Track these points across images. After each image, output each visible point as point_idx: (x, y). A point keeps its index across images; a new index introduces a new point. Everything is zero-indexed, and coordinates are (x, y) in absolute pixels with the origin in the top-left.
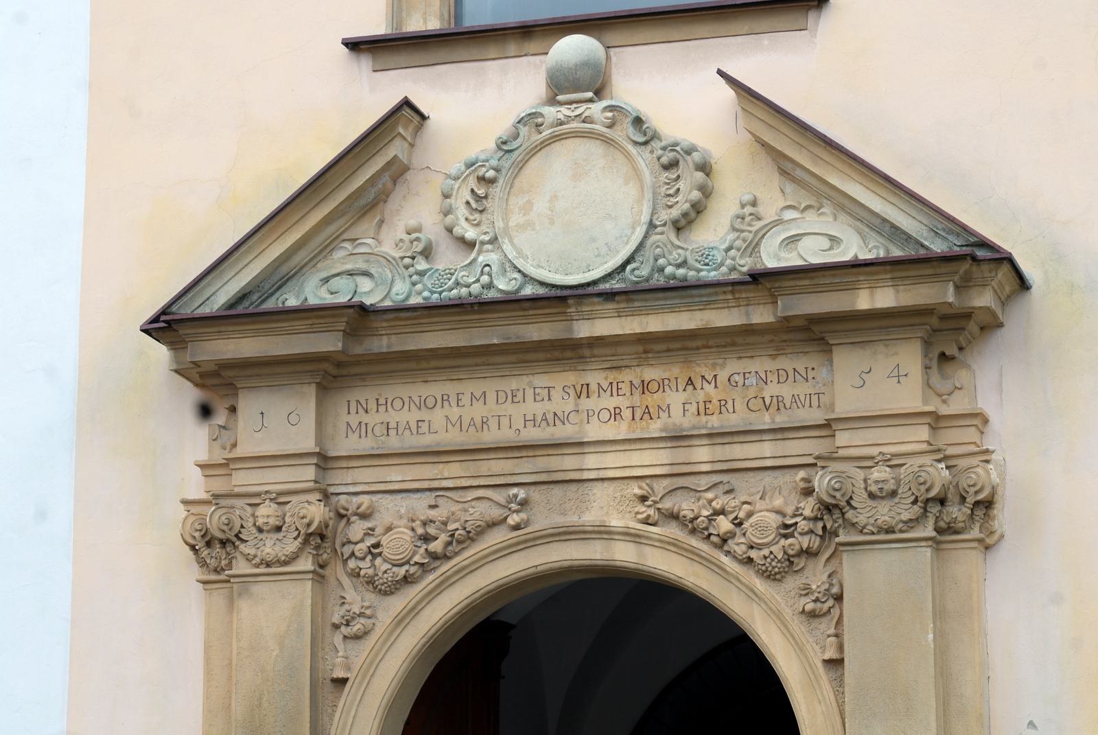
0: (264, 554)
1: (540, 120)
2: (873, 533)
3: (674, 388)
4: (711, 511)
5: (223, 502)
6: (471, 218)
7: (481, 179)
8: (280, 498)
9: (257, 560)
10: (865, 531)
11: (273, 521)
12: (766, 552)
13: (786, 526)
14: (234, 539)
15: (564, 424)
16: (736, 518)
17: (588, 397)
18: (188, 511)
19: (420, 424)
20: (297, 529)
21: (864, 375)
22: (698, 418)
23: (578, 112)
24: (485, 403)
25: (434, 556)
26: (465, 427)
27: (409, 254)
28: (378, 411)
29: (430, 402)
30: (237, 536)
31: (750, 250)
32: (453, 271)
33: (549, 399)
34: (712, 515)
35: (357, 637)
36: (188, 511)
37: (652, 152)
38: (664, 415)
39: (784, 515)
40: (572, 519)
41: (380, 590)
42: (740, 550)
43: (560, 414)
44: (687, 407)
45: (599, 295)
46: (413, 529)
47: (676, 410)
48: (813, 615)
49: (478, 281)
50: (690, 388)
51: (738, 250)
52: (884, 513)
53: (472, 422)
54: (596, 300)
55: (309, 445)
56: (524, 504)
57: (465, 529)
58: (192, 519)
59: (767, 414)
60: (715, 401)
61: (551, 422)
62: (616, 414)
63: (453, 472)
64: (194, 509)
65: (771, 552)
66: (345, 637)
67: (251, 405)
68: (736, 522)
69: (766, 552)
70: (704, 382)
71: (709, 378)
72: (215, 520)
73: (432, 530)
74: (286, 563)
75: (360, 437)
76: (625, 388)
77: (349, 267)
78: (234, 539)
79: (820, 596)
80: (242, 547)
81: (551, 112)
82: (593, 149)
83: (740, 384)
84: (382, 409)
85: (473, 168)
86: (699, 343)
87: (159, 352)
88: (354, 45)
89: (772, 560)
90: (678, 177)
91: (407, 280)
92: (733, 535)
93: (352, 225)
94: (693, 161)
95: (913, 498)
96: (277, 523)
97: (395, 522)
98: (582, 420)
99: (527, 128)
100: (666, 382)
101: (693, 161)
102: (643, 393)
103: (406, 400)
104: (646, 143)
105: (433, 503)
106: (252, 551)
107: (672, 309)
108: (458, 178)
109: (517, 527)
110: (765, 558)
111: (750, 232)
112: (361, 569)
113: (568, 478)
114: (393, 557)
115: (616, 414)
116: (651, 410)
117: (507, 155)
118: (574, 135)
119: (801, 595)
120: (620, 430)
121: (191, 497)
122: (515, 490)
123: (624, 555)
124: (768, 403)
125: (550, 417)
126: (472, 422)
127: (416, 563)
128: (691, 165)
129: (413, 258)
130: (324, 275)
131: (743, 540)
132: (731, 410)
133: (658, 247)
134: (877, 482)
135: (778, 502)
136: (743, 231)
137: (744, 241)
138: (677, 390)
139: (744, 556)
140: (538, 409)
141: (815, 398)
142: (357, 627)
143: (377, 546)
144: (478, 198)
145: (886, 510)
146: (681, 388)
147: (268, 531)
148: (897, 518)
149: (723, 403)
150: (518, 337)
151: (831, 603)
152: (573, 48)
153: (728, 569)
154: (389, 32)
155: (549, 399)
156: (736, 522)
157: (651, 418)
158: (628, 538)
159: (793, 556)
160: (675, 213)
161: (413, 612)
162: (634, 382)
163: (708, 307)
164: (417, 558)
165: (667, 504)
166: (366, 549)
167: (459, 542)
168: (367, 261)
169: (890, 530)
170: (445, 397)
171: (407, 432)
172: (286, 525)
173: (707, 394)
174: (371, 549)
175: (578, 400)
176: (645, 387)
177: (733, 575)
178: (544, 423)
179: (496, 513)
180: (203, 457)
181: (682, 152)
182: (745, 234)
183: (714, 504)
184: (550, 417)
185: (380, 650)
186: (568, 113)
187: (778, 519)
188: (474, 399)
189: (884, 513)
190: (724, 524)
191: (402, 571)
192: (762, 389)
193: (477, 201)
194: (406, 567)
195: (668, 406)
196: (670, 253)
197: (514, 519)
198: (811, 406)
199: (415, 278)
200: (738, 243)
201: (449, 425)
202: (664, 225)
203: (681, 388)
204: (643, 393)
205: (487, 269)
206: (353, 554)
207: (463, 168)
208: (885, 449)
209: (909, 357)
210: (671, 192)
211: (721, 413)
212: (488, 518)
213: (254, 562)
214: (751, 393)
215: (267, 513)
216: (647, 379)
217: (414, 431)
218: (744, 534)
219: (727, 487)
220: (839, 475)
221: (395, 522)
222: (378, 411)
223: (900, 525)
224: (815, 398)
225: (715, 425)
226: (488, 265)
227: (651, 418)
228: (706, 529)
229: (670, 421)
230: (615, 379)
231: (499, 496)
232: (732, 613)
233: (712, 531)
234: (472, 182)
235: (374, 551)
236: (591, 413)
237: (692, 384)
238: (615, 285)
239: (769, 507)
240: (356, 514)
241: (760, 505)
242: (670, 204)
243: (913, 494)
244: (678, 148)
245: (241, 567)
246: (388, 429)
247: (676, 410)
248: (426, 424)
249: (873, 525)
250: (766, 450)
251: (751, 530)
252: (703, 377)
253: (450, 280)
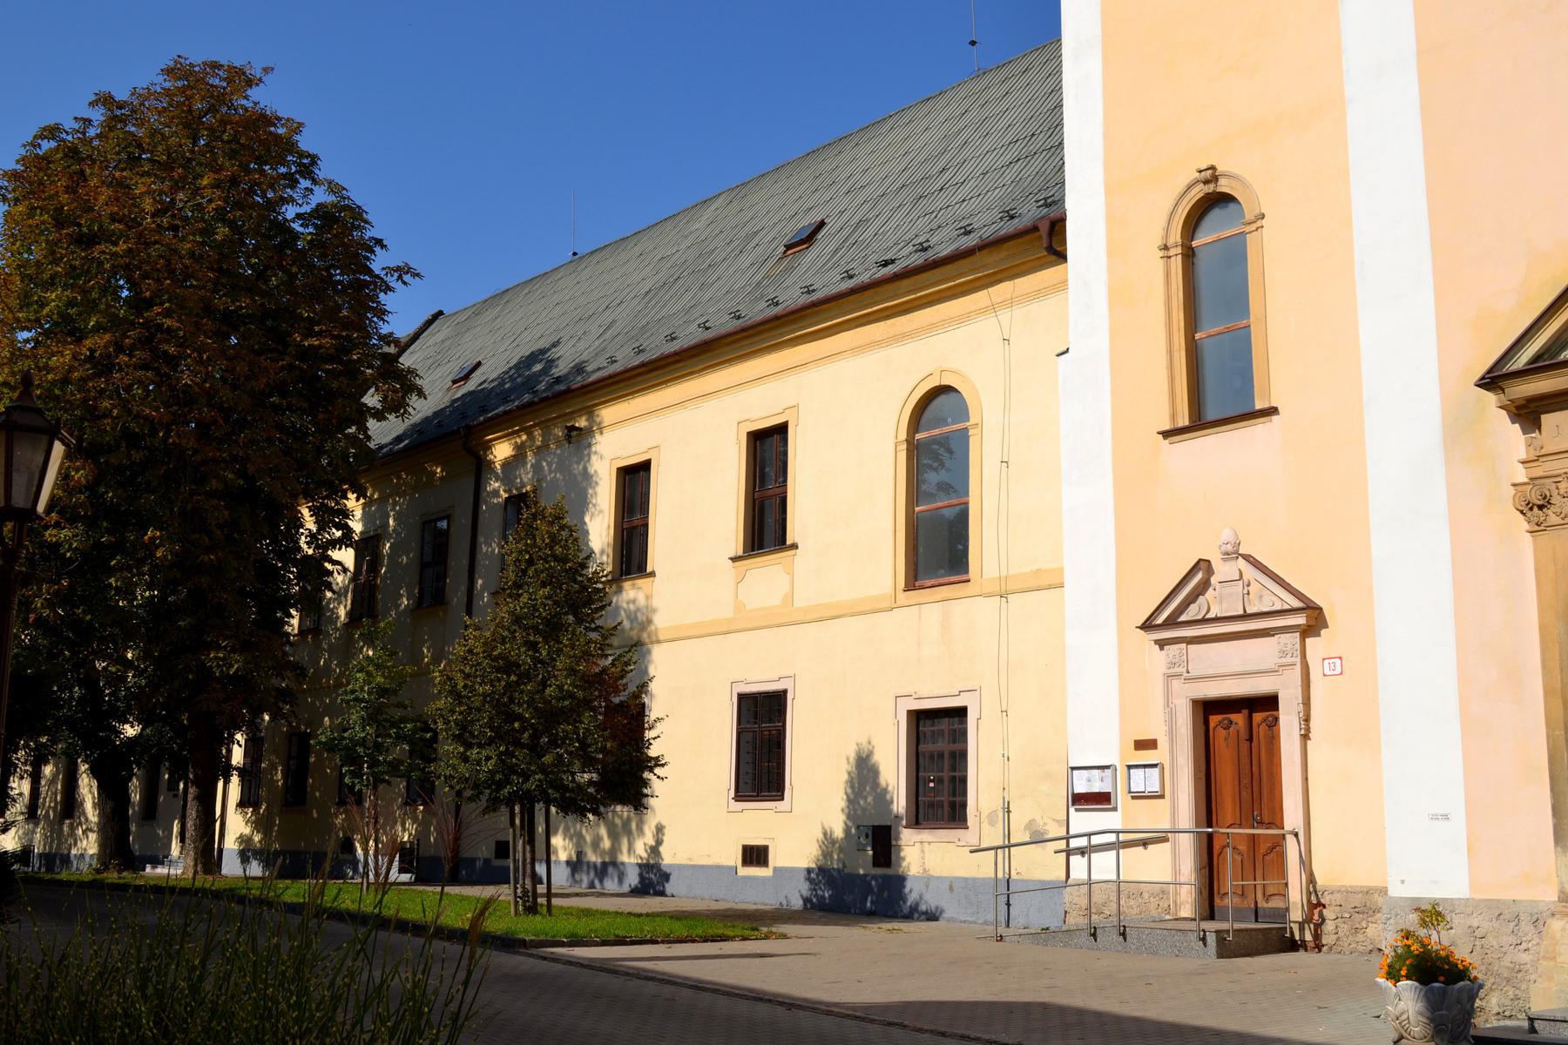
87: (1490, 398)
180: (1523, 456)
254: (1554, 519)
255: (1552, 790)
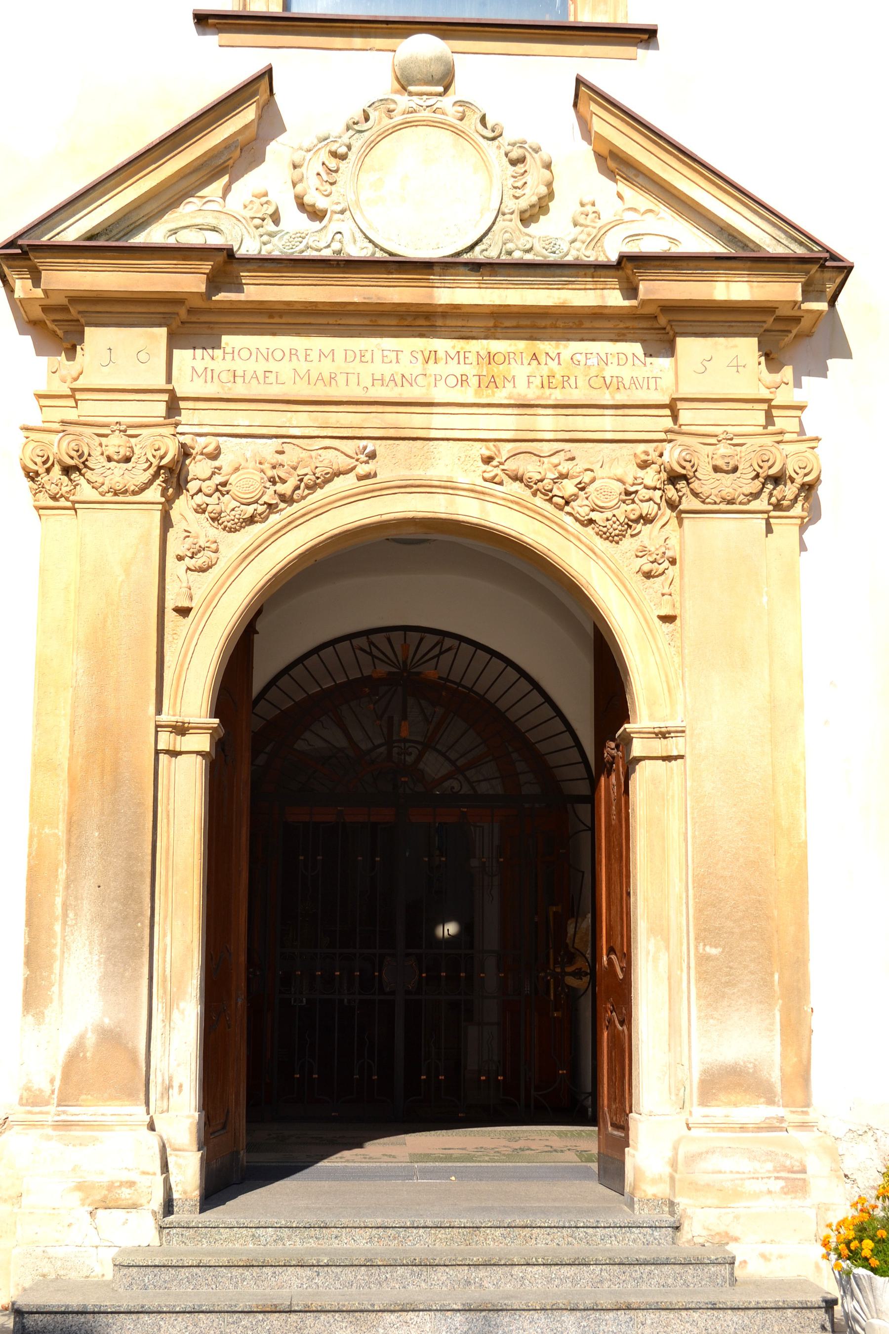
0: (113, 482)
1: (392, 106)
2: (715, 503)
3: (520, 363)
4: (557, 475)
5: (71, 429)
6: (321, 188)
7: (334, 154)
8: (127, 431)
9: (105, 488)
10: (708, 500)
11: (123, 452)
12: (609, 514)
13: (628, 493)
14: (81, 466)
15: (411, 385)
16: (580, 483)
17: (436, 363)
18: (27, 438)
19: (267, 374)
20: (148, 460)
21: (705, 363)
22: (542, 390)
23: (429, 103)
24: (333, 361)
25: (283, 498)
26: (313, 381)
27: (260, 215)
28: (224, 358)
29: (278, 355)
30: (83, 463)
31: (593, 243)
32: (303, 235)
33: (398, 362)
34: (557, 478)
35: (202, 570)
36: (27, 438)
37: (499, 147)
38: (509, 385)
39: (624, 483)
40: (418, 473)
41: (230, 528)
42: (583, 512)
43: (408, 376)
44: (531, 379)
45: (466, 264)
46: (262, 471)
47: (521, 382)
48: (648, 575)
49: (329, 246)
50: (535, 362)
51: (583, 242)
52: (727, 485)
53: (320, 377)
54: (462, 269)
55: (160, 382)
56: (372, 456)
57: (314, 474)
58: (32, 445)
59: (607, 392)
60: (558, 376)
61: (399, 383)
62: (463, 380)
63: (300, 420)
64: (33, 435)
65: (614, 516)
66: (188, 569)
67: (96, 338)
68: (579, 486)
69: (609, 514)
70: (548, 358)
71: (553, 355)
72: (61, 448)
73: (282, 473)
74: (134, 493)
75: (206, 382)
76: (472, 358)
77: (199, 221)
78: (81, 466)
79: (658, 557)
80: (88, 474)
81: (403, 102)
82: (446, 136)
83: (583, 362)
84: (229, 357)
85: (326, 142)
86: (548, 322)
88: (203, 20)
89: (614, 523)
90: (526, 171)
91: (257, 237)
92: (576, 497)
93: (130, 212)
94: (542, 160)
95: (755, 473)
96: (128, 454)
97: (244, 464)
98: (429, 384)
99: (377, 113)
100: (512, 355)
101: (542, 160)
102: (490, 363)
103: (254, 352)
104: (493, 139)
105: (280, 449)
106: (100, 480)
107: (531, 286)
108: (310, 151)
109: (360, 478)
110: (608, 520)
111: (595, 228)
112: (207, 505)
113: (415, 436)
114: (242, 496)
115: (463, 380)
116: (497, 380)
117: (357, 135)
118: (425, 123)
119: (637, 556)
120: (468, 395)
121: (31, 424)
122: (363, 443)
123: (467, 510)
124: (608, 382)
125: (398, 378)
126: (320, 377)
127: (265, 503)
128: (539, 163)
129: (263, 220)
130: (173, 226)
131: (586, 502)
132: (573, 386)
133: (506, 232)
134: (724, 456)
135: (619, 472)
136: (587, 226)
137: (589, 235)
138: (522, 364)
139: (587, 518)
140: (387, 370)
141: (652, 381)
142: (201, 560)
143: (224, 484)
144: (330, 171)
145: (729, 483)
146: (526, 362)
147: (118, 462)
148: (740, 490)
149: (566, 379)
150: (379, 298)
151: (666, 564)
152: (424, 47)
153: (570, 529)
154: (236, 9)
155: (398, 362)
156: (579, 486)
157: (497, 387)
158: (472, 495)
159: (632, 521)
160: (524, 203)
161: (258, 548)
162: (481, 353)
163: (566, 286)
164: (265, 498)
165: (511, 465)
166: (214, 487)
167: (308, 487)
168: (216, 218)
169: (731, 502)
170: (293, 352)
171: (254, 381)
172: (136, 456)
173: (551, 370)
174: (219, 487)
175: (426, 365)
176: (491, 358)
177: (573, 534)
178: (392, 384)
179: (343, 462)
181: (530, 150)
182: (589, 229)
183: (560, 468)
184: (398, 378)
185: (223, 584)
186: (421, 102)
187: (618, 487)
188: (322, 356)
189: (727, 485)
190: (569, 487)
191: (250, 510)
192: (603, 369)
193: (328, 174)
194: (255, 506)
195: (514, 377)
196: (518, 239)
197: (362, 469)
198: (648, 388)
199: (265, 238)
200: (583, 237)
201: (297, 378)
202: (512, 213)
203: (526, 362)
204: (490, 363)
205: (338, 236)
206: (200, 490)
207: (316, 142)
208: (730, 429)
209: (746, 348)
210: (519, 184)
211: (563, 387)
212: (335, 467)
213: (100, 490)
214: (593, 372)
215: (115, 444)
216: (493, 352)
217: (262, 381)
218: (587, 498)
219: (569, 455)
220: (687, 448)
221: (244, 464)
222: (224, 358)
223: (742, 497)
224: (652, 381)
225: (559, 398)
226: (340, 233)
227: (497, 387)
228: (551, 491)
229: (515, 391)
230: (462, 348)
231: (350, 447)
232: (570, 570)
233: (556, 491)
234: (324, 156)
235: (222, 488)
236: (438, 378)
237: (537, 359)
238: (477, 255)
239: (612, 475)
240: (202, 454)
241: (599, 473)
242: (517, 195)
243: (754, 470)
244: (526, 146)
245: (86, 492)
246: (235, 376)
247: (521, 382)
248: (274, 375)
249: (716, 496)
250: (607, 423)
251: (596, 493)
252: (547, 354)
253: (301, 242)
254: (86, 492)
255: (29, 923)
